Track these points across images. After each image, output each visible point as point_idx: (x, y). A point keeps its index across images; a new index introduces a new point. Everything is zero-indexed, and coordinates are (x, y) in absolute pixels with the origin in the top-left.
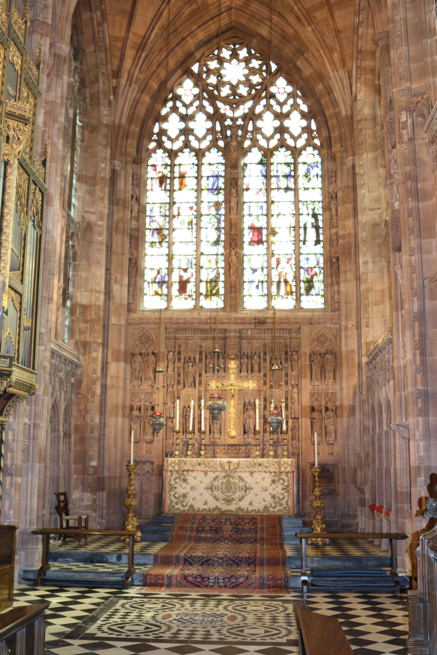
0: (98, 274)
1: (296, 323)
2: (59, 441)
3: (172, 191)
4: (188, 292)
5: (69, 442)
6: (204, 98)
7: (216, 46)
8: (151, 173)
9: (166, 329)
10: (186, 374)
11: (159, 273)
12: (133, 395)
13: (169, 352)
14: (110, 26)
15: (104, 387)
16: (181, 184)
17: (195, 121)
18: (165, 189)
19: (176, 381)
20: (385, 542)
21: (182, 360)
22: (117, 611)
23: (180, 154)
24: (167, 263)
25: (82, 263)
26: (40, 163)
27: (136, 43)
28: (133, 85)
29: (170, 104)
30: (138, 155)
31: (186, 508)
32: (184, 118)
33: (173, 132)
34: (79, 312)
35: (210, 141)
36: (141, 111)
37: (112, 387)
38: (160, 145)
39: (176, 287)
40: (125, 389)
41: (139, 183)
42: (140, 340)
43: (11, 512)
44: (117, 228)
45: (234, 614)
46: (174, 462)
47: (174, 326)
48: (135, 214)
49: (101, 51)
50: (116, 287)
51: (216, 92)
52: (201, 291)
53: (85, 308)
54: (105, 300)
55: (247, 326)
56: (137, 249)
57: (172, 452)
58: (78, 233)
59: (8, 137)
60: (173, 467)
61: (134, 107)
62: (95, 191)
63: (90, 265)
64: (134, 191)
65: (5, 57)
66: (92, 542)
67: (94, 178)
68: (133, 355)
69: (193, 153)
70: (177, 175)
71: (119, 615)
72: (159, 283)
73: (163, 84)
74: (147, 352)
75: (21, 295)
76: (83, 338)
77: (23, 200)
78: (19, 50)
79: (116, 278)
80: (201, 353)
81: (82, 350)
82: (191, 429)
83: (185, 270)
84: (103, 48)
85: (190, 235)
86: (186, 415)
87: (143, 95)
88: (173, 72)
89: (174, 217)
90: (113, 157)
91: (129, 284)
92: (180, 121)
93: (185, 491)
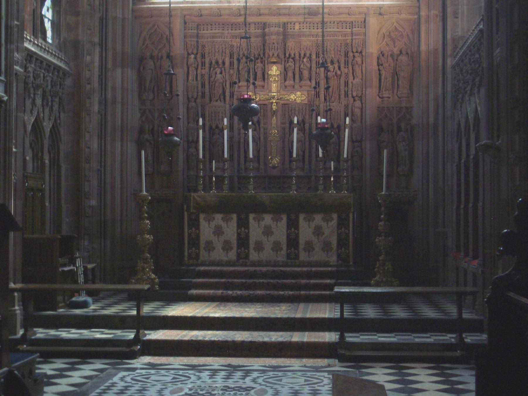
1: (360, 13)
2: (43, 172)
9: (185, 23)
13: (189, 54)
19: (200, 94)
20: (188, 39)
21: (207, 65)
22: (113, 385)
45: (264, 387)
55: (294, 19)
74: (160, 55)
80: (231, 56)
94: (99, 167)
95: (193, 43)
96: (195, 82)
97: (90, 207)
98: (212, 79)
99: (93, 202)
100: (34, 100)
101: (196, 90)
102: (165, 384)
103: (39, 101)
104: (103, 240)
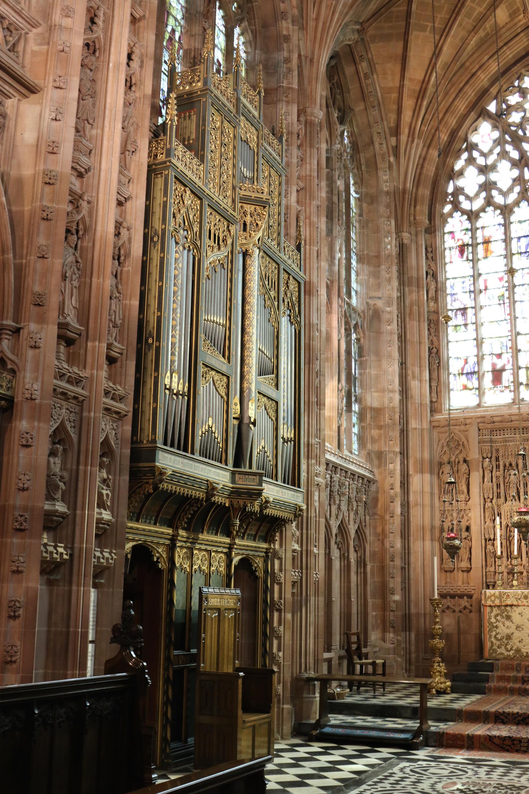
0: (390, 370)
3: (474, 261)
4: (505, 383)
5: (365, 573)
6: (507, 142)
7: (517, 76)
8: (449, 242)
9: (479, 430)
10: (507, 485)
11: (466, 362)
12: (443, 513)
14: (380, 76)
15: (406, 506)
16: (487, 250)
17: (497, 172)
18: (468, 259)
19: (495, 494)
21: (502, 468)
22: (391, 775)
23: (482, 214)
24: (476, 349)
25: (370, 358)
26: (293, 247)
27: (414, 90)
28: (416, 140)
29: (465, 156)
30: (430, 223)
31: (511, 653)
32: (483, 170)
33: (471, 189)
34: (370, 417)
35: (519, 193)
36: (430, 170)
37: (416, 505)
38: (456, 206)
39: (488, 378)
40: (432, 506)
41: (434, 255)
42: (448, 445)
43: (281, 654)
44: (411, 314)
46: (494, 595)
47: (489, 426)
48: (432, 293)
49: (373, 107)
50: (414, 384)
51: (520, 133)
52: (520, 381)
53: (378, 412)
54: (401, 401)
56: (438, 336)
57: (495, 582)
58: (361, 325)
59: (245, 225)
60: (493, 602)
61: (421, 166)
62: (379, 272)
63: (380, 361)
64: (429, 266)
65: (235, 137)
66: (391, 692)
67: (378, 257)
68: (441, 464)
69: (498, 211)
70: (480, 240)
71: (392, 780)
72: (467, 374)
73: (453, 134)
75: (277, 403)
76: (376, 448)
77: (271, 293)
78: (252, 125)
79: (413, 373)
81: (376, 462)
82: (516, 553)
83: (499, 356)
84: (376, 104)
85: (501, 312)
86: (510, 536)
87: (431, 151)
88: (464, 117)
89: (481, 291)
90: (399, 230)
91: (430, 379)
92: (479, 175)
93: (508, 631)
94: (403, 565)
95: (487, 448)
96: (490, 484)
97: (394, 601)
98: (506, 480)
99: (397, 597)
100: (339, 506)
101: (491, 491)
102: (440, 778)
103: (344, 507)
104: (408, 633)
